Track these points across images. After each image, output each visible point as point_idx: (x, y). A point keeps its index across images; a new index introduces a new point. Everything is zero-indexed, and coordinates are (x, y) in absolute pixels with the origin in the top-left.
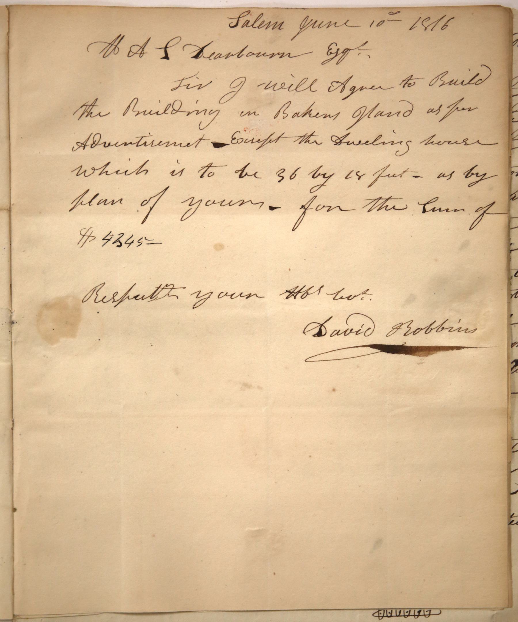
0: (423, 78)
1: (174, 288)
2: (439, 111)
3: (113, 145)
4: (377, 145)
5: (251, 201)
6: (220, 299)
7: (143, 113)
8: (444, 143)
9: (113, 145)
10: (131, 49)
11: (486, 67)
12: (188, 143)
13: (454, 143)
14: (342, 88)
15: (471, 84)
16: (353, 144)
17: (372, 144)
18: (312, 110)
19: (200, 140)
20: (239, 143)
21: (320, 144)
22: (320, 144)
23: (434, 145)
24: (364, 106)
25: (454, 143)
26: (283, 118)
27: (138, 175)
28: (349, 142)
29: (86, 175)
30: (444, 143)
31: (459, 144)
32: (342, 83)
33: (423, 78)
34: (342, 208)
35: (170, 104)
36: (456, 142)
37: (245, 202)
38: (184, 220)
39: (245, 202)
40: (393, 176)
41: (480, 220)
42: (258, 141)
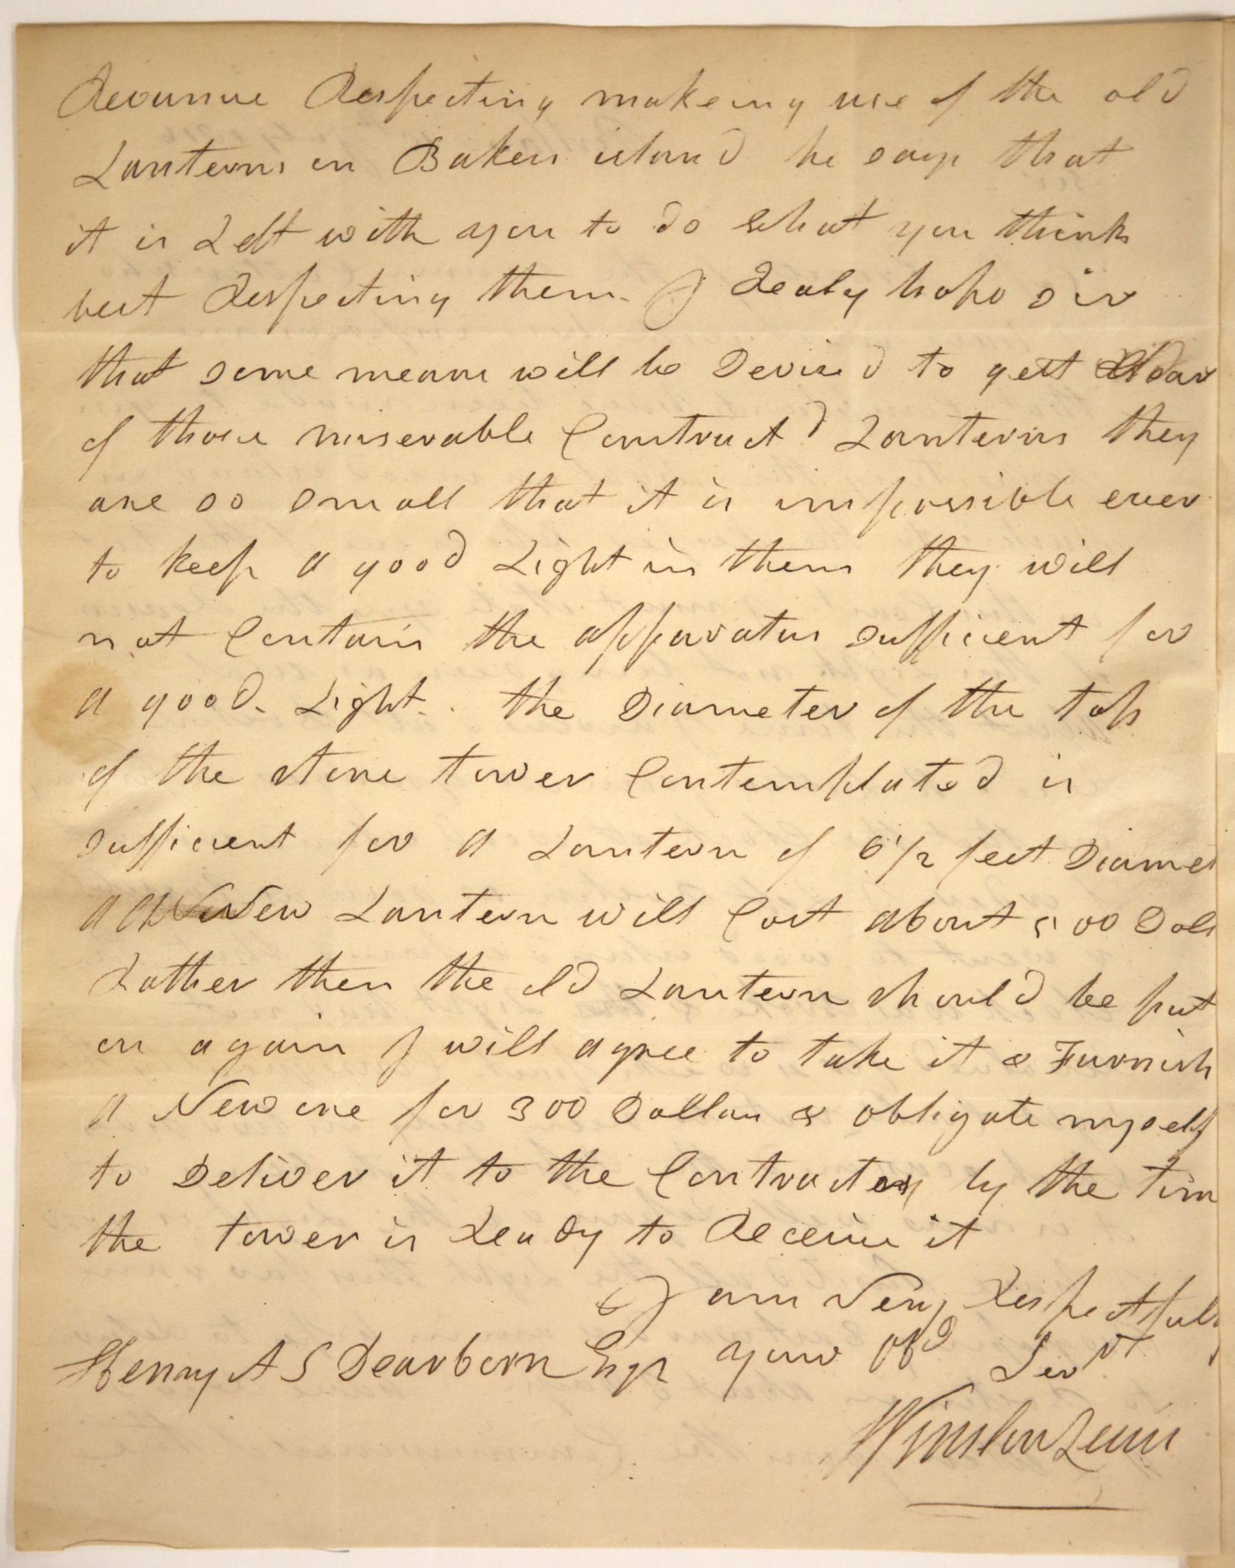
0: (626, 1305)
1: (1000, 692)
6: (259, 367)
7: (510, 777)
11: (716, 1226)
14: (1102, 562)
15: (533, 922)
18: (1050, 1333)
19: (483, 1169)
24: (1070, 1116)
26: (330, 1343)
29: (274, 1099)
32: (1079, 628)
33: (626, 1305)
35: (175, 571)
37: (476, 437)
38: (149, 165)
39: (476, 437)
41: (644, 706)
42: (926, 158)
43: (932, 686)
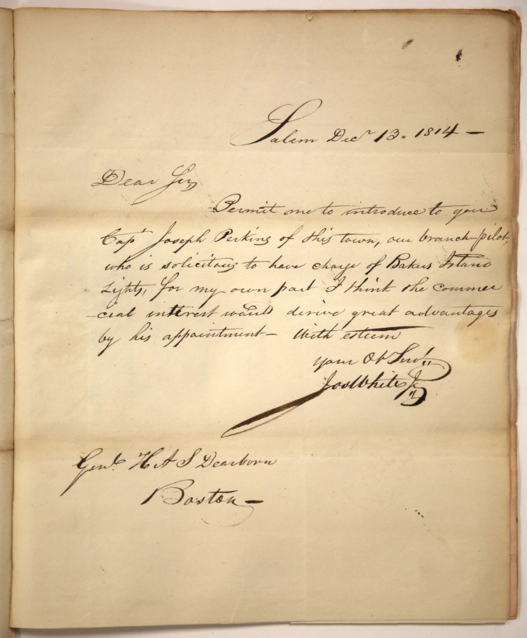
40: (300, 314)
43: (62, 495)
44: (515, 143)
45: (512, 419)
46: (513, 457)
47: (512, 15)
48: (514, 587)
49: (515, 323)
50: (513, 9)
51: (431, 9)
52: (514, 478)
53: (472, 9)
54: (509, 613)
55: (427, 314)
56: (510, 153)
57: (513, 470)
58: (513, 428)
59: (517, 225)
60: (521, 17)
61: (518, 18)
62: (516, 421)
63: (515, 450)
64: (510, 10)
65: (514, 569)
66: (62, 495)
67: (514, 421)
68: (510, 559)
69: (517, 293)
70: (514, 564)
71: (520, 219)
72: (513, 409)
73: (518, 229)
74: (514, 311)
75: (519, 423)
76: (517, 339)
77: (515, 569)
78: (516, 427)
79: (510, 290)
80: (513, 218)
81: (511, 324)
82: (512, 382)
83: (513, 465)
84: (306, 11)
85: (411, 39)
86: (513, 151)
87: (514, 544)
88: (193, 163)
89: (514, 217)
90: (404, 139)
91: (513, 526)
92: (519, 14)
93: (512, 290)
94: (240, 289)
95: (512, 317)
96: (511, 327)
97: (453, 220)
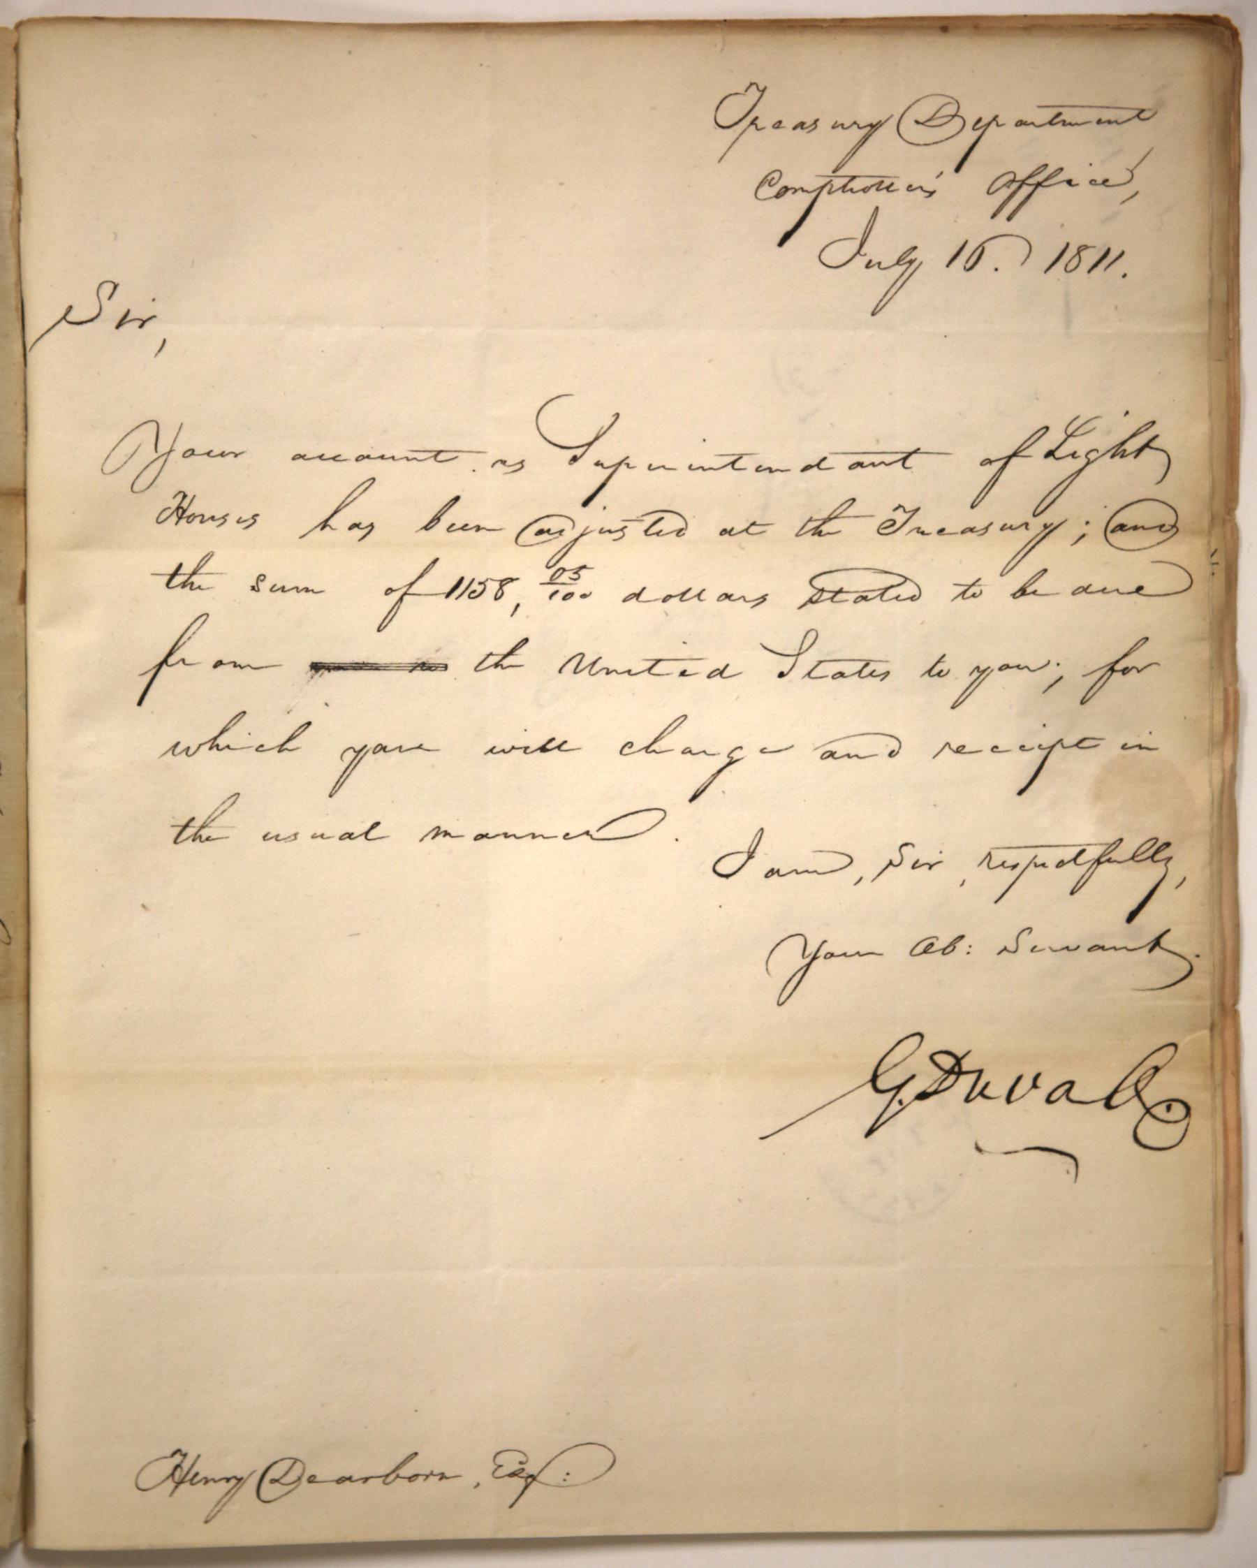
2: (1080, 261)
3: (393, 750)
4: (530, 524)
5: (743, 597)
8: (199, 748)
9: (393, 750)
10: (1131, 175)
12: (802, 120)
13: (842, 757)
16: (1139, 669)
17: (1150, 859)
20: (944, 951)
21: (101, 310)
22: (101, 310)
23: (786, 877)
25: (842, 757)
27: (801, 537)
28: (353, 834)
30: (199, 748)
31: (1171, 1125)
34: (518, 835)
36: (208, 454)
43: (462, 836)
44: (1231, 337)
45: (1228, 1000)
46: (1230, 1091)
47: (1223, 29)
48: (1234, 1402)
49: (1233, 766)
50: (1222, 14)
51: (1026, 16)
52: (1232, 1140)
53: (1125, 13)
54: (1226, 1464)
55: (1013, 1098)
56: (1220, 360)
57: (1232, 1123)
58: (1229, 1021)
59: (1235, 530)
60: (1239, 30)
61: (1235, 33)
62: (1236, 1002)
63: (1233, 1074)
64: (1216, 17)
65: (1235, 1359)
66: (462, 836)
67: (1231, 1003)
68: (1226, 1334)
69: (1236, 693)
70: (1234, 1347)
71: (1244, 514)
72: (1229, 973)
73: (1238, 539)
74: (1230, 740)
75: (1244, 1007)
76: (1237, 802)
77: (1237, 1359)
78: (1236, 1014)
79: (1222, 689)
80: (1228, 518)
81: (1224, 771)
82: (1226, 911)
83: (1231, 1110)
84: (725, 21)
85: (1204, 619)
86: (1227, 354)
87: (1233, 1299)
88: (135, 495)
89: (1229, 514)
90: (363, 1485)
91: (1232, 1256)
92: (1235, 23)
93: (1225, 689)
94: (521, 746)
95: (1226, 753)
96: (1224, 778)
97: (1081, 541)
